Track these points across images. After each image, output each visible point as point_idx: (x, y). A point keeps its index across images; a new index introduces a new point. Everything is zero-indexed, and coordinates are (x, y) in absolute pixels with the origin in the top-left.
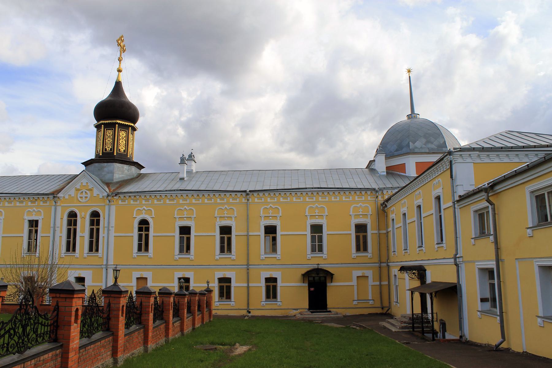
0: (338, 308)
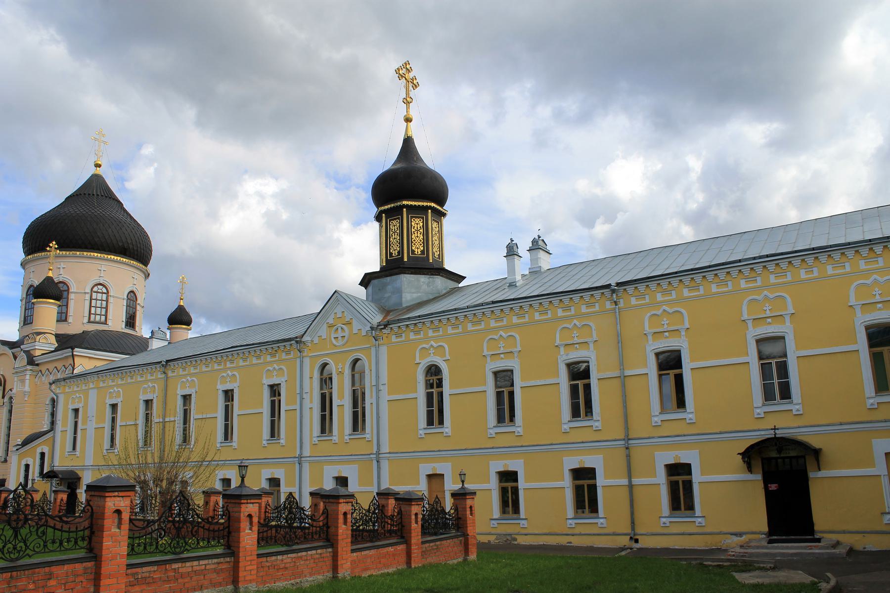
0: (844, 532)
